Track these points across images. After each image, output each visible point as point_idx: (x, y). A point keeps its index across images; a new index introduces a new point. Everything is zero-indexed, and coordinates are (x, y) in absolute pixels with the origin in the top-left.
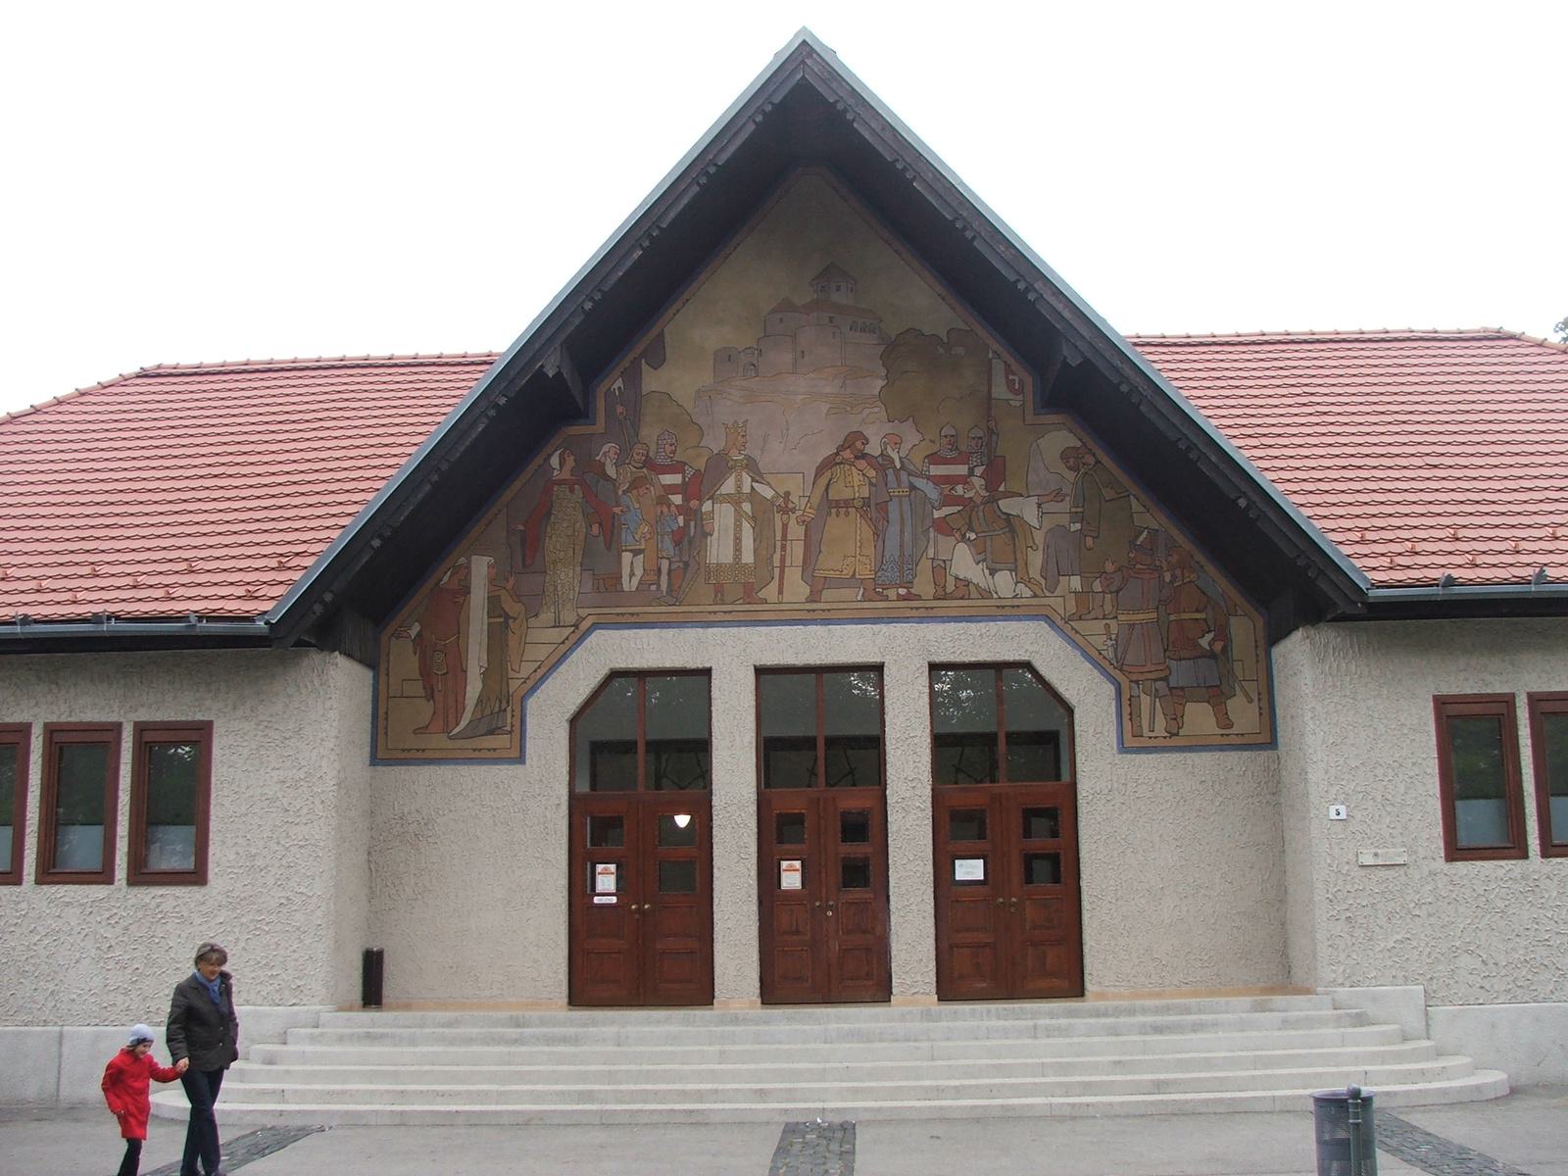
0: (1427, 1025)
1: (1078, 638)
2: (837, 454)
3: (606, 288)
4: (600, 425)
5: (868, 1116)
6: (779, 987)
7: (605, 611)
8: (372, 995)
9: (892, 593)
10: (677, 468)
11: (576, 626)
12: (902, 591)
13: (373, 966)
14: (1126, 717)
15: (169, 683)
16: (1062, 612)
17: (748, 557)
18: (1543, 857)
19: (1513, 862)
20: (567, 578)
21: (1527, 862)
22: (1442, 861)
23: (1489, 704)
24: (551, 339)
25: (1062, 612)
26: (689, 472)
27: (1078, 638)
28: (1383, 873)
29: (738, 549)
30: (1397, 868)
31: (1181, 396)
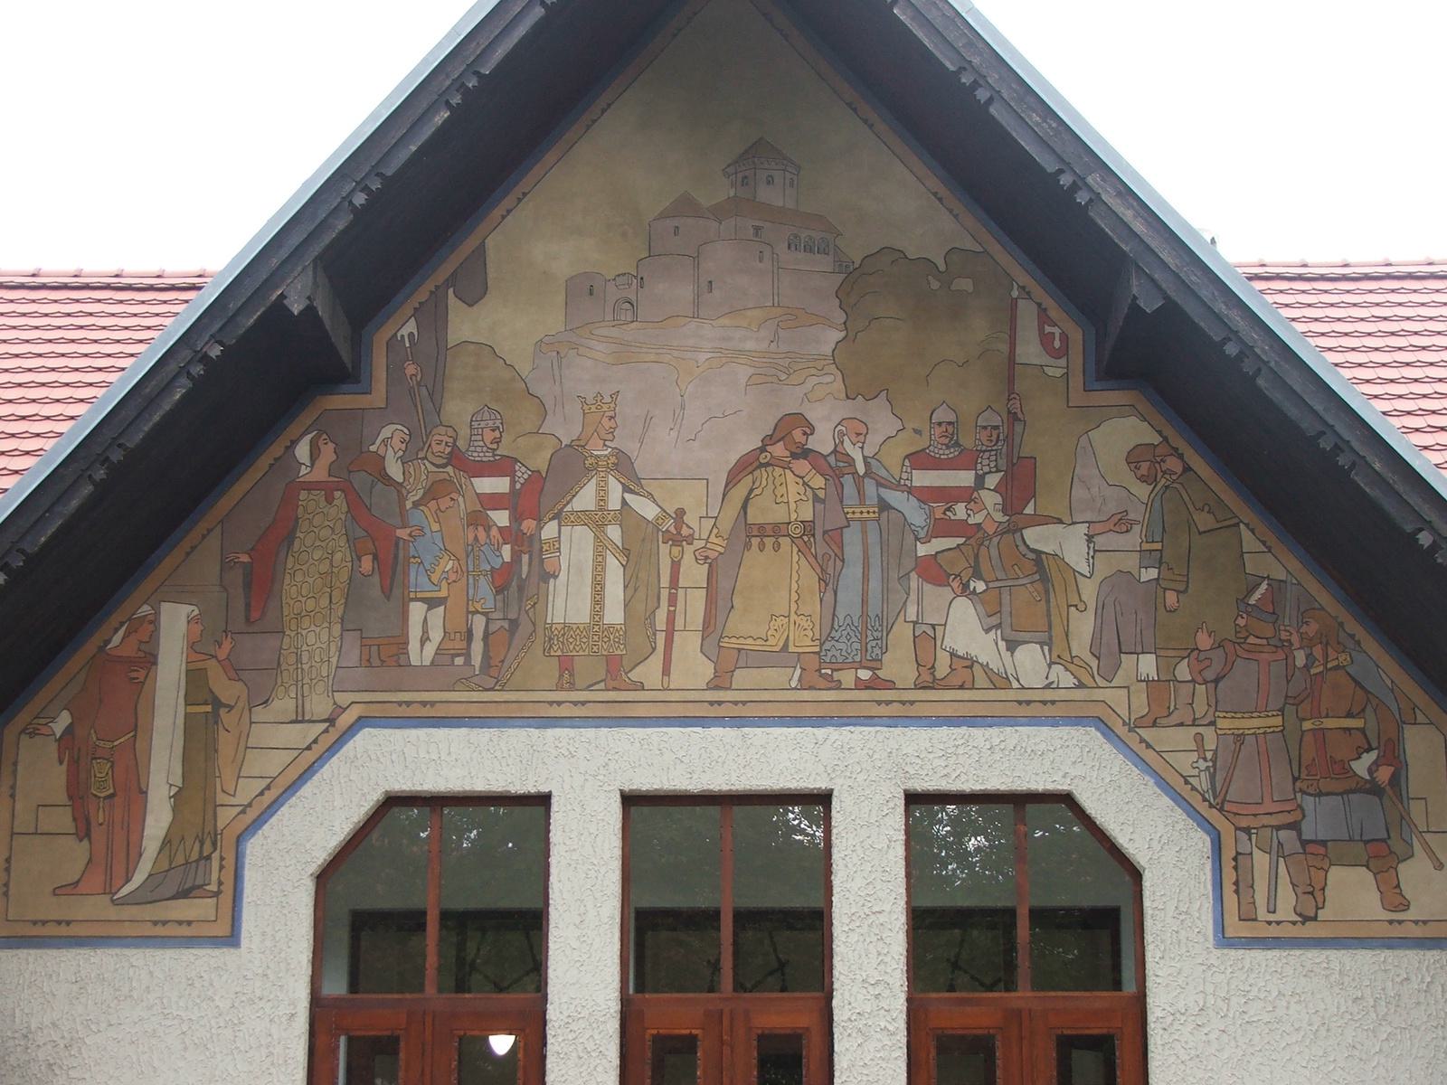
1: (1149, 755)
9: (847, 677)
10: (502, 466)
11: (331, 721)
17: (614, 614)
25: (1124, 713)
26: (522, 474)
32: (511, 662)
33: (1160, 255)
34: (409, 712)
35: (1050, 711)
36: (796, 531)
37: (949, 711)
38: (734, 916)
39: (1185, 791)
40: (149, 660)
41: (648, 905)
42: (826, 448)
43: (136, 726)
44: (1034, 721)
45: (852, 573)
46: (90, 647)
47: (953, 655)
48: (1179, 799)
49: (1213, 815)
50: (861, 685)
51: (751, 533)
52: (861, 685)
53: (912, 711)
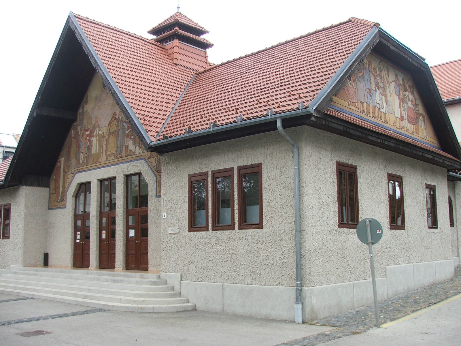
0: (180, 287)
1: (149, 164)
2: (111, 120)
3: (41, 93)
4: (78, 123)
5: (38, 297)
6: (128, 266)
7: (78, 169)
8: (46, 263)
9: (118, 156)
10: (88, 130)
11: (74, 173)
12: (120, 155)
13: (46, 256)
14: (158, 186)
15: (403, 171)
16: (147, 156)
17: (98, 151)
18: (390, 229)
19: (205, 232)
20: (73, 161)
21: (208, 232)
22: (187, 232)
23: (202, 176)
24: (34, 108)
25: (147, 156)
26: (90, 130)
27: (149, 164)
28: (174, 236)
29: (96, 151)
30: (177, 234)
31: (119, 90)
32: (92, 163)
33: (88, 45)
34: (80, 170)
35: (140, 158)
36: (114, 132)
37: (130, 159)
38: (147, 202)
39: (153, 169)
40: (61, 167)
41: (96, 198)
42: (117, 118)
43: (59, 177)
44: (137, 160)
45: (120, 138)
46: (56, 167)
47: (129, 150)
48: (151, 169)
49: (156, 173)
50: (121, 157)
51: (110, 134)
52: (121, 157)
53: (126, 160)
